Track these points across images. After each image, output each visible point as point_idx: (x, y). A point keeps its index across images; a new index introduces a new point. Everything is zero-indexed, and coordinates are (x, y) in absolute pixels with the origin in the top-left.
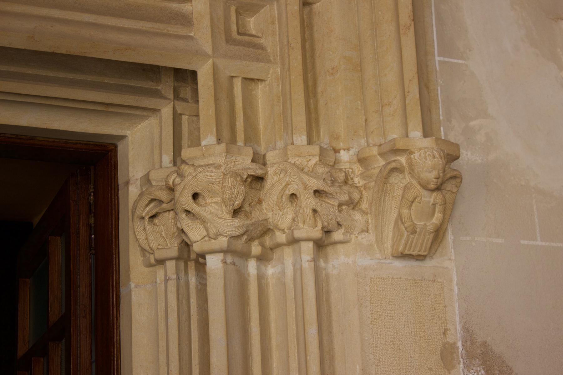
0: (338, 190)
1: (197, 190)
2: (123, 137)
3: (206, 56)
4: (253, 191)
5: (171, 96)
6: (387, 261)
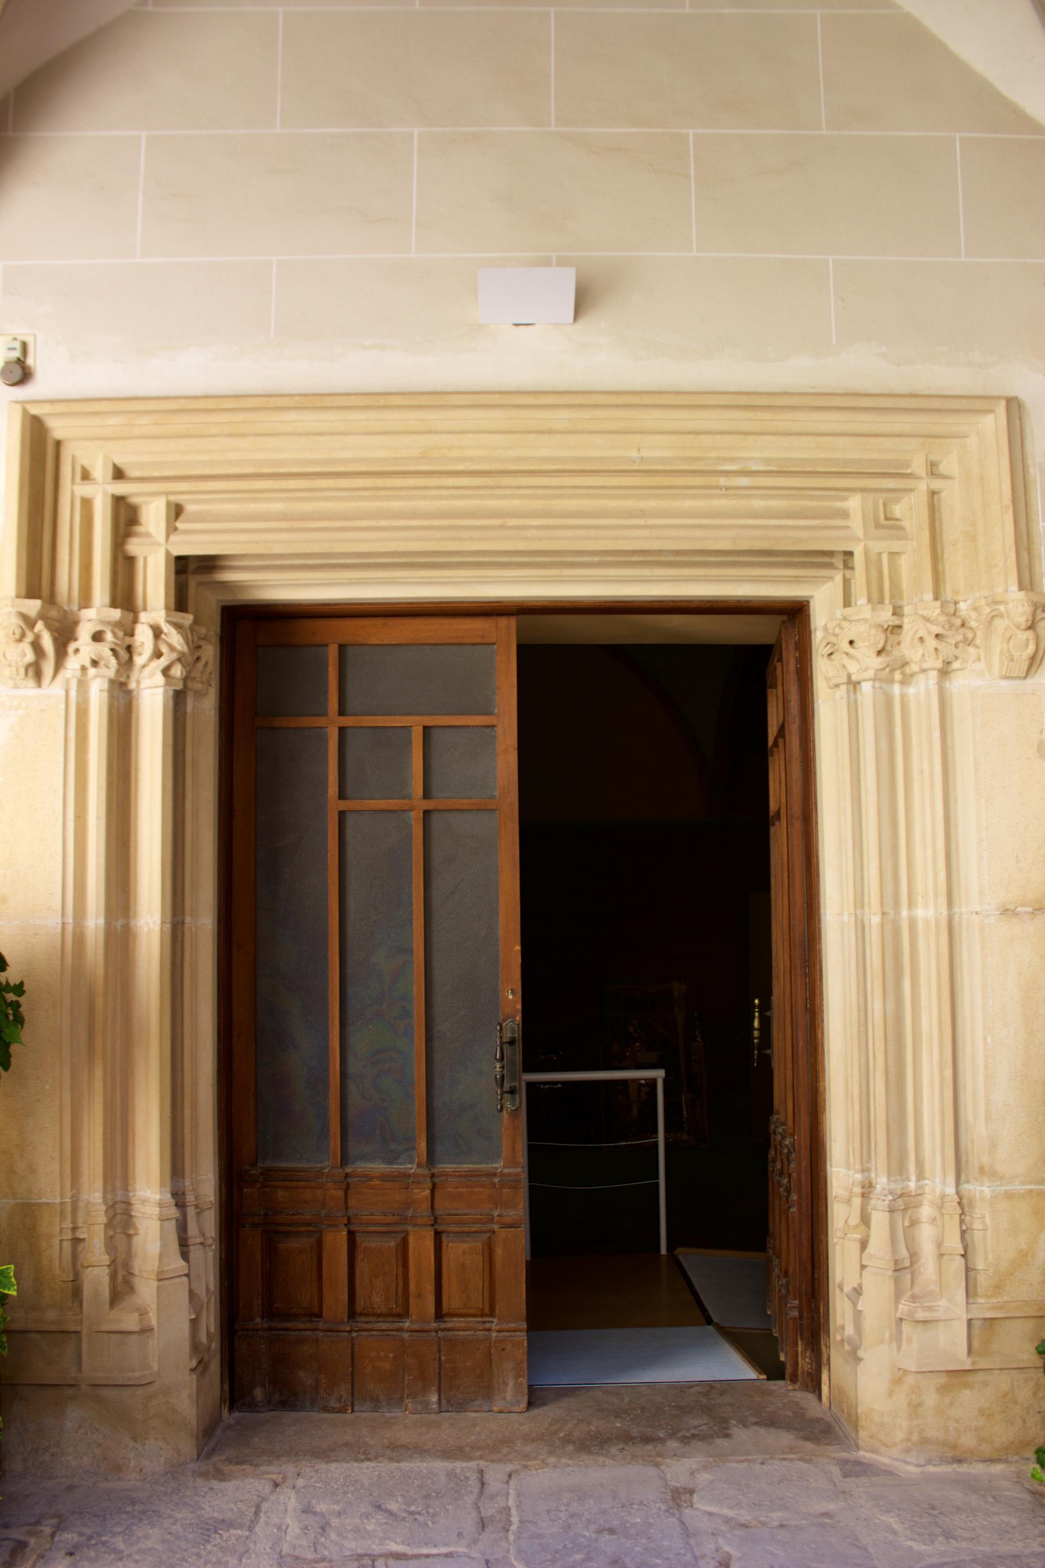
0: (954, 632)
1: (852, 638)
2: (812, 597)
3: (858, 540)
4: (894, 636)
5: (841, 566)
6: (996, 682)
